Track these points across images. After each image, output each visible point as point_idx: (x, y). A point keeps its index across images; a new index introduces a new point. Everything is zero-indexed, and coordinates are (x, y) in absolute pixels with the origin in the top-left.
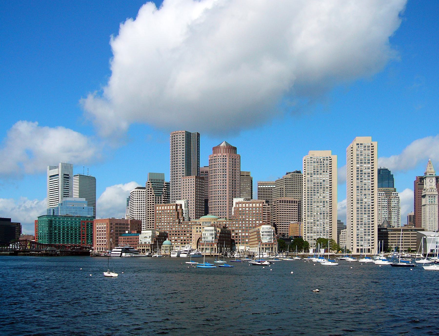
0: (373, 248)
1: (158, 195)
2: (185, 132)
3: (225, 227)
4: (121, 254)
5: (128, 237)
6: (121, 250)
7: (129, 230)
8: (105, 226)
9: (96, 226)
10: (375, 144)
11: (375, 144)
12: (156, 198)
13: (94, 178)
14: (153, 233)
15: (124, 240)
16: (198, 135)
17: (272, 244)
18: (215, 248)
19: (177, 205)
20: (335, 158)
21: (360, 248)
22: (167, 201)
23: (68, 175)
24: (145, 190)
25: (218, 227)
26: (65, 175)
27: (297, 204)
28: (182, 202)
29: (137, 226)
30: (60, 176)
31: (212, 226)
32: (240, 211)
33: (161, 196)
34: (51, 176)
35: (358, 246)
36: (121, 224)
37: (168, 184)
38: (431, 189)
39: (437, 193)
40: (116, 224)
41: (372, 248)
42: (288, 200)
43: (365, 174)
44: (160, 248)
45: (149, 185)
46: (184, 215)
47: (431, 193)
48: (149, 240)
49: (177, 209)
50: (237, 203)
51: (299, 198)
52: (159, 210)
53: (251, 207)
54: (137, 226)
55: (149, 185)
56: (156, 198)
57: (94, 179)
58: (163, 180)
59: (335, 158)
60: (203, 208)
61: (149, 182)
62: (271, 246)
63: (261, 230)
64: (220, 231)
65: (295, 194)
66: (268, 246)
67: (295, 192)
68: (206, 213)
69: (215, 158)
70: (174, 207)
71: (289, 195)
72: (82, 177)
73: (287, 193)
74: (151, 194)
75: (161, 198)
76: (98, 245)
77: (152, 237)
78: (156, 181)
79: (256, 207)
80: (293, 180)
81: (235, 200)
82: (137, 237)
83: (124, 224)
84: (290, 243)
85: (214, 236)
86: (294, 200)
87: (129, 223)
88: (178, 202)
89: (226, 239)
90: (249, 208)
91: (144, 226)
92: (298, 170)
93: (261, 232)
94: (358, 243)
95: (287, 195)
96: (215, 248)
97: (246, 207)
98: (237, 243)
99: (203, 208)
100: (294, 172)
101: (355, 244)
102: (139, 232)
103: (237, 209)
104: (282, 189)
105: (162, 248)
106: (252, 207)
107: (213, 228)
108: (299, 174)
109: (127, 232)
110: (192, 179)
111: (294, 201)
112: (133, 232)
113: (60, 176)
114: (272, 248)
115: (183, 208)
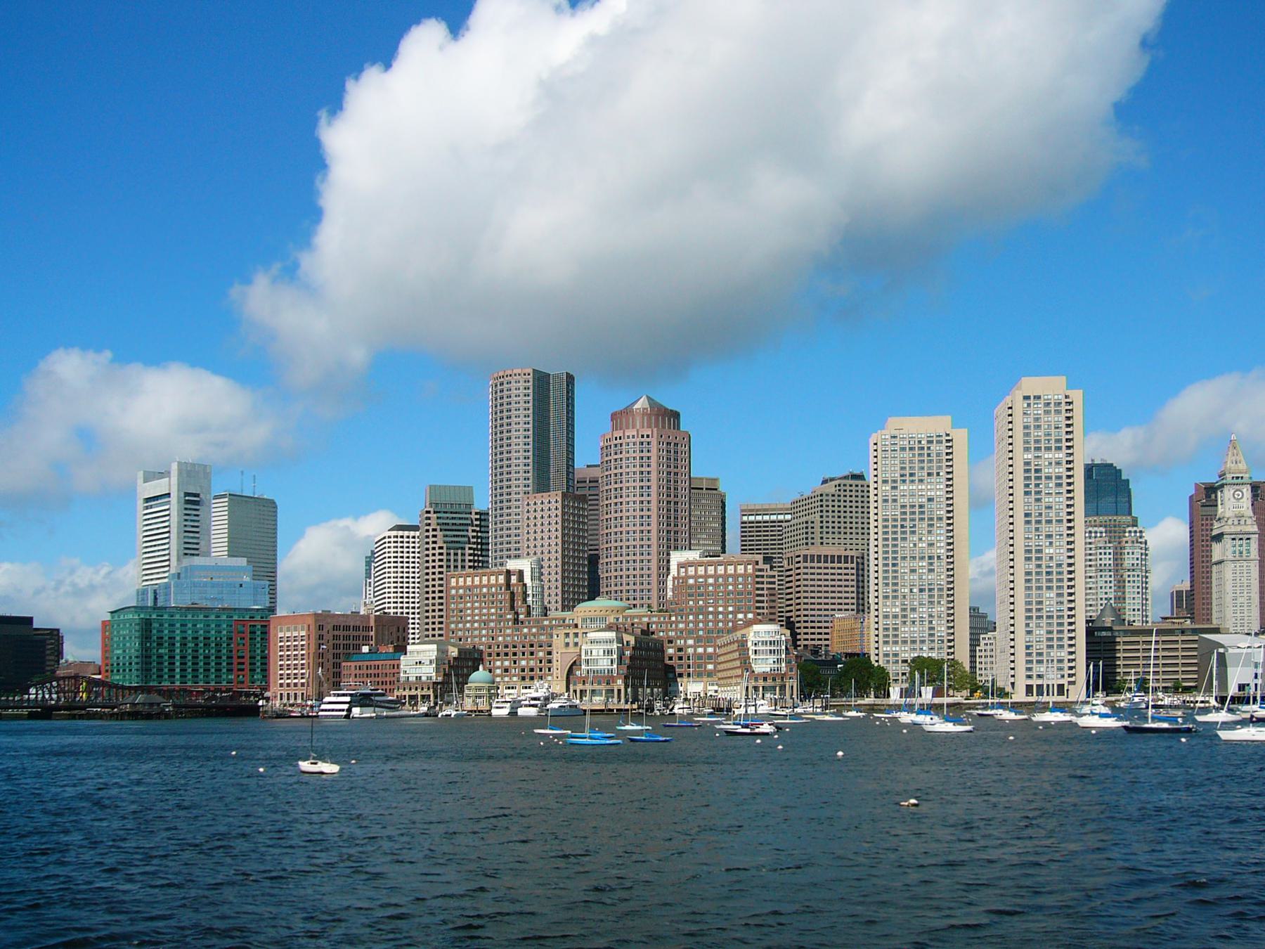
1: (454, 546)
2: (530, 371)
4: (349, 710)
6: (348, 699)
9: (276, 635)
13: (272, 504)
14: (442, 651)
15: (358, 672)
16: (570, 379)
18: (619, 691)
19: (509, 573)
20: (961, 437)
21: (1035, 682)
22: (480, 562)
23: (197, 495)
24: (417, 533)
26: (187, 494)
27: (854, 565)
29: (394, 633)
30: (174, 499)
32: (691, 587)
34: (147, 500)
35: (1029, 677)
36: (347, 628)
37: (483, 516)
38: (1240, 517)
39: (1255, 529)
40: (335, 628)
42: (829, 553)
43: (1048, 478)
44: (461, 691)
45: (429, 518)
46: (530, 599)
47: (1238, 529)
48: (429, 672)
49: (508, 585)
50: (680, 566)
51: (860, 547)
53: (721, 576)
54: (394, 633)
55: (429, 518)
56: (448, 554)
57: (269, 507)
58: (470, 505)
60: (584, 578)
61: (428, 512)
62: (778, 681)
63: (751, 638)
64: (632, 643)
66: (770, 683)
69: (619, 441)
70: (502, 579)
71: (831, 541)
72: (237, 501)
74: (434, 542)
75: (463, 554)
76: (281, 685)
77: (439, 661)
78: (448, 508)
81: (677, 557)
82: (396, 662)
83: (356, 628)
86: (844, 553)
88: (512, 565)
91: (414, 630)
92: (857, 472)
95: (825, 541)
96: (619, 691)
97: (706, 576)
98: (681, 675)
99: (584, 578)
100: (845, 478)
102: (401, 649)
103: (681, 582)
105: (466, 692)
106: (726, 576)
107: (612, 635)
108: (860, 482)
109: (365, 649)
112: (383, 649)
113: (174, 499)
114: (783, 688)
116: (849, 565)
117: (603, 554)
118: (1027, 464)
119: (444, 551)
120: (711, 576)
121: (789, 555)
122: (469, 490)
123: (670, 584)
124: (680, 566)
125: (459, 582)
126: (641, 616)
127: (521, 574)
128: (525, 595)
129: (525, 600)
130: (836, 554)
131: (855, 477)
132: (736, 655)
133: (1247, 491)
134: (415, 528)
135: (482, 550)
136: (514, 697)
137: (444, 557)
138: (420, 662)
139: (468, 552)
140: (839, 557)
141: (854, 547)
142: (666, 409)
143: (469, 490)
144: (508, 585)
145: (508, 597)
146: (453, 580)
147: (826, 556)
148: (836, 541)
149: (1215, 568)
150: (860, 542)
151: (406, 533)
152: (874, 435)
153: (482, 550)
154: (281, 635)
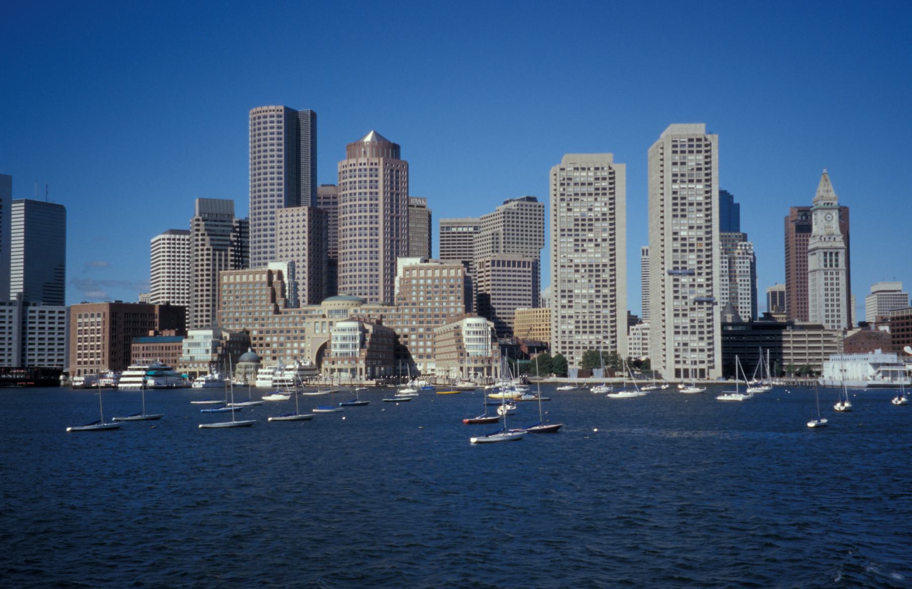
0: (713, 367)
1: (218, 248)
2: (282, 108)
3: (379, 322)
4: (145, 382)
5: (168, 345)
6: (144, 373)
7: (157, 328)
8: (99, 319)
9: (75, 321)
10: (714, 140)
11: (714, 140)
12: (214, 255)
13: (61, 210)
14: (217, 336)
15: (145, 352)
16: (313, 115)
17: (489, 360)
18: (361, 369)
19: (270, 273)
20: (621, 171)
21: (681, 366)
22: (241, 261)
24: (187, 237)
25: (365, 321)
27: (530, 269)
28: (281, 266)
29: (174, 319)
31: (352, 319)
33: (226, 250)
35: (677, 362)
37: (243, 226)
41: (709, 368)
42: (512, 259)
43: (691, 204)
44: (234, 368)
45: (198, 225)
46: (287, 294)
49: (270, 283)
50: (406, 269)
51: (533, 254)
52: (229, 285)
53: (437, 278)
54: (174, 319)
55: (198, 225)
56: (214, 255)
57: (61, 210)
58: (231, 216)
59: (621, 171)
60: (324, 280)
61: (198, 220)
62: (486, 364)
63: (465, 329)
64: (371, 331)
65: (524, 246)
66: (479, 365)
67: (524, 241)
68: (332, 292)
69: (353, 168)
70: (265, 278)
71: (511, 249)
72: (31, 207)
73: (507, 245)
74: (203, 245)
75: (226, 255)
76: (79, 363)
77: (215, 345)
78: (219, 218)
79: (448, 278)
80: (520, 216)
81: (402, 263)
82: (177, 344)
84: (521, 355)
85: (358, 342)
86: (522, 260)
87: (157, 312)
88: (273, 266)
89: (389, 353)
90: (433, 279)
91: (190, 317)
92: (531, 195)
93: (464, 333)
94: (677, 356)
95: (507, 249)
96: (361, 369)
99: (324, 280)
100: (522, 199)
101: (671, 359)
102: (182, 333)
103: (407, 283)
104: (495, 236)
105: (238, 369)
106: (441, 278)
107: (355, 324)
108: (533, 203)
109: (151, 333)
110: (300, 215)
111: (524, 263)
112: (166, 333)
114: (489, 369)
115: (286, 280)
116: (526, 269)
117: (341, 257)
118: (675, 193)
119: (211, 252)
120: (422, 278)
121: (481, 260)
122: (230, 203)
123: (397, 284)
124: (406, 269)
125: (230, 278)
126: (373, 310)
127: (280, 274)
128: (283, 291)
129: (283, 295)
130: (517, 259)
131: (530, 199)
132: (140, 379)
133: (835, 215)
134: (187, 232)
135: (241, 252)
136: (268, 377)
137: (211, 257)
138: (198, 345)
139: (230, 253)
140: (519, 262)
141: (529, 254)
142: (390, 143)
143: (230, 203)
144: (270, 283)
145: (269, 292)
146: (225, 278)
147: (509, 262)
148: (515, 249)
149: (810, 276)
150: (533, 250)
151: (177, 237)
152: (553, 168)
153: (241, 252)
154: (80, 320)
